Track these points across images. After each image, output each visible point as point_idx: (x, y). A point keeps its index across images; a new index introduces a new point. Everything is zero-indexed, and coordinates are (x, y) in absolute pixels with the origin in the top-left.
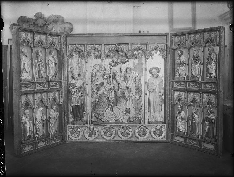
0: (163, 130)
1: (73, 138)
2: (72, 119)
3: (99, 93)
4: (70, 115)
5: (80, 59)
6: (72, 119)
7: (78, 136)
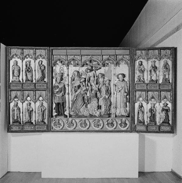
0: (127, 122)
1: (56, 128)
2: (56, 114)
3: (77, 93)
4: (54, 111)
5: (62, 66)
6: (56, 114)
7: (59, 127)
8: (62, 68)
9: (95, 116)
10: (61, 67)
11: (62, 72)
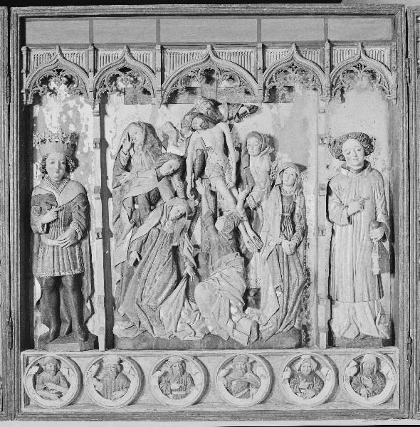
5: (72, 103)
7: (60, 395)
8: (70, 113)
9: (232, 344)
10: (66, 108)
11: (72, 129)
